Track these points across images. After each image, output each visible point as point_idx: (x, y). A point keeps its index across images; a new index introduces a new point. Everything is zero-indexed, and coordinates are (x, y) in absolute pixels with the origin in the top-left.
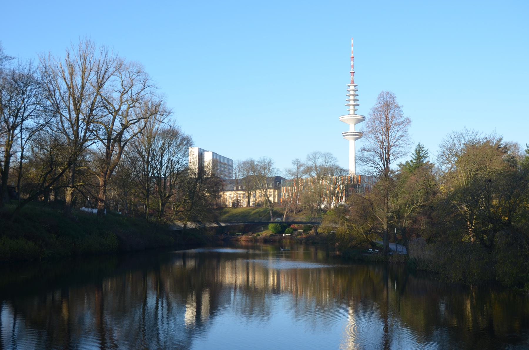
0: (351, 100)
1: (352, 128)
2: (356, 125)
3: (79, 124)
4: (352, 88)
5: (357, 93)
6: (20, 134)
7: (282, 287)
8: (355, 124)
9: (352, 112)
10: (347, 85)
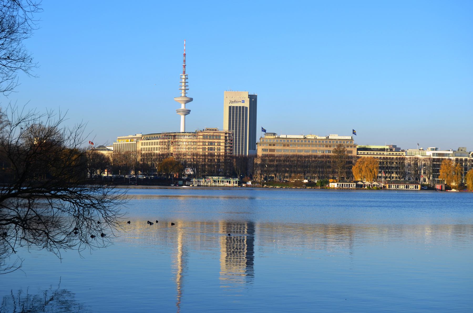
0: (183, 86)
1: (183, 107)
2: (186, 116)
3: (4, 219)
4: (184, 77)
5: (187, 88)
6: (13, 246)
7: (470, 181)
8: (185, 104)
9: (183, 95)
10: (181, 75)
